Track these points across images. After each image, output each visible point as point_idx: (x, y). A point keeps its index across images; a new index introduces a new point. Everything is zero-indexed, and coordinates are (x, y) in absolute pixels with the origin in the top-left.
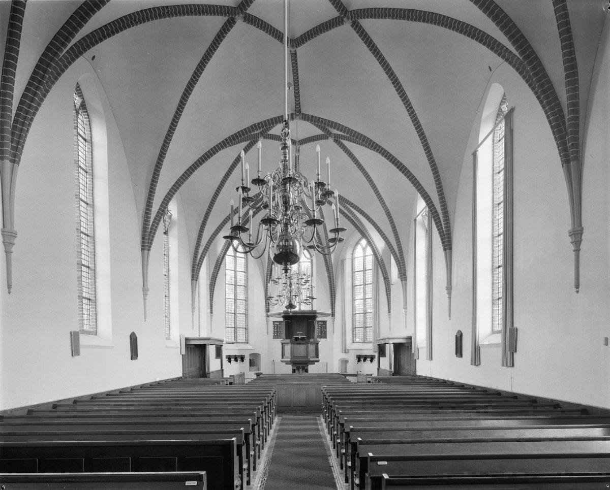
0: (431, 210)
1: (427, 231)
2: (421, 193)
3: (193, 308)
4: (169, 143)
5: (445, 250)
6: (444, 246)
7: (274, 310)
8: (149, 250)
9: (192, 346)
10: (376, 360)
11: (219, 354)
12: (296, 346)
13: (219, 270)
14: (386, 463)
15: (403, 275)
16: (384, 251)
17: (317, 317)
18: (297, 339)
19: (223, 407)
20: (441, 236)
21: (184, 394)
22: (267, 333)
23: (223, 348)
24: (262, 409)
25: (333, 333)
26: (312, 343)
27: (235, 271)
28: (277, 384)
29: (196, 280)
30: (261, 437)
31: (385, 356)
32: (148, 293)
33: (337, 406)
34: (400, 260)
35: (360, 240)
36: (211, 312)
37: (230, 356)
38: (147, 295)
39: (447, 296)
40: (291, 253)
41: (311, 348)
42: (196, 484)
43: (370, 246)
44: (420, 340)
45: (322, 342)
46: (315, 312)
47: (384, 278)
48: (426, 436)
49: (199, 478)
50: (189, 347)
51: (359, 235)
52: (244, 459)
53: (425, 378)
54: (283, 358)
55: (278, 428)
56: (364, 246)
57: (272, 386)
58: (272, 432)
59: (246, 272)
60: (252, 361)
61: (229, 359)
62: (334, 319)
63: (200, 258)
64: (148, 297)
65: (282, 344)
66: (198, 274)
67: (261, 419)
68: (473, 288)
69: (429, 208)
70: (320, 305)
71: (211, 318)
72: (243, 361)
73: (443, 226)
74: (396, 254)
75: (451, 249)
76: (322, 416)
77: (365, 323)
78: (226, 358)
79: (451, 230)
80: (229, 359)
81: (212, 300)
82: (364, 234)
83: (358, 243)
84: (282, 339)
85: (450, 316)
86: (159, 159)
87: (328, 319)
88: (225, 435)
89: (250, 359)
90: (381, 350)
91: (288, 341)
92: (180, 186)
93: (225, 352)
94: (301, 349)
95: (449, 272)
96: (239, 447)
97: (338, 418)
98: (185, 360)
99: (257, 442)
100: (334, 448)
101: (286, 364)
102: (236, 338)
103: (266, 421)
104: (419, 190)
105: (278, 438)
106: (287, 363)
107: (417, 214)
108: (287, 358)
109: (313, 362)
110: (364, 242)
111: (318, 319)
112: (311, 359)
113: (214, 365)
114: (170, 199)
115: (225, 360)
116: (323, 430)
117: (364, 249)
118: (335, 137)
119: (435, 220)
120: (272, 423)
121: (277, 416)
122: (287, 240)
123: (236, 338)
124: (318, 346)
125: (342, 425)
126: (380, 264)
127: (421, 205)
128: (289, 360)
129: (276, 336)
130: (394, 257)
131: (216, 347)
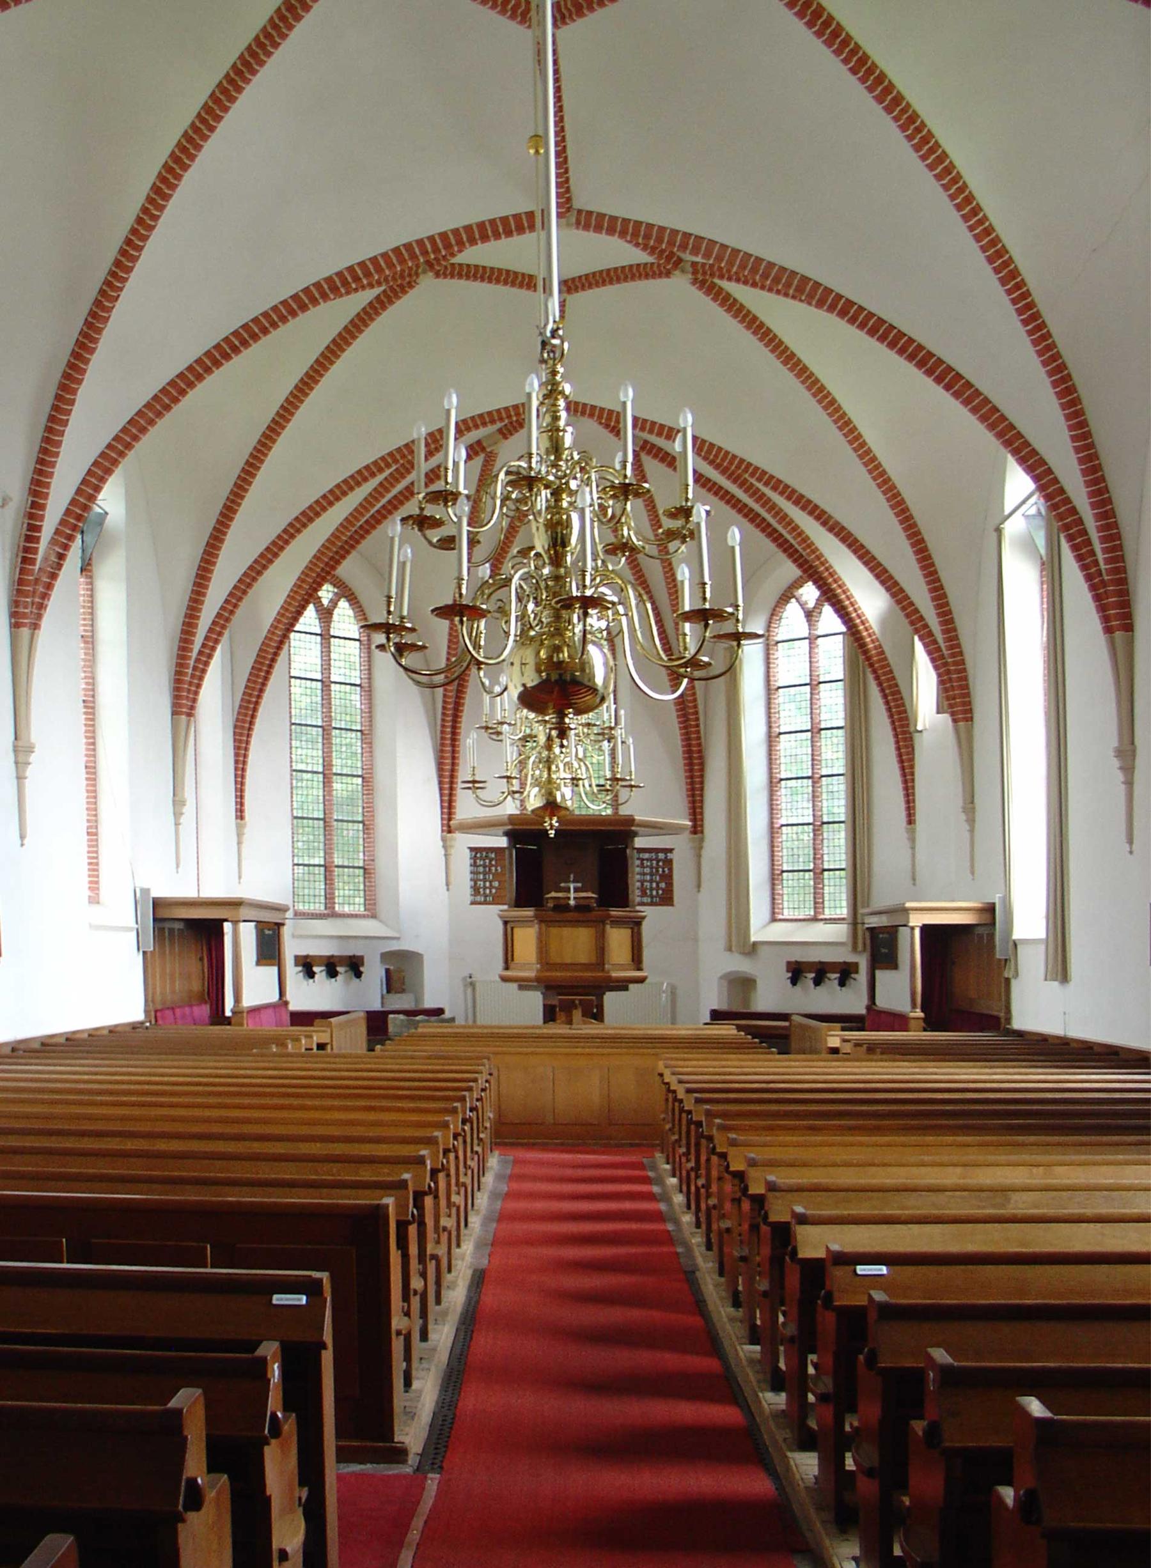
0: (1053, 507)
1: (1043, 564)
2: (1015, 452)
3: (178, 803)
4: (109, 310)
5: (1108, 630)
6: (1106, 619)
7: (467, 808)
8: (35, 626)
9: (180, 926)
10: (862, 977)
11: (269, 949)
12: (554, 931)
13: (266, 679)
14: (884, 1270)
15: (957, 697)
16: (884, 622)
17: (635, 834)
18: (561, 907)
19: (317, 1115)
20: (1093, 588)
21: (172, 1075)
22: (447, 884)
23: (286, 932)
24: (456, 1127)
25: (699, 886)
26: (618, 922)
27: (326, 684)
28: (496, 1054)
29: (190, 715)
30: (415, 1302)
31: (895, 966)
32: (33, 758)
33: (718, 1121)
34: (946, 652)
35: (798, 584)
36: (240, 814)
37: (307, 957)
38: (182, 814)
39: (1120, 777)
40: (575, 682)
41: (618, 939)
42: (304, 1302)
43: (833, 605)
44: (1028, 921)
45: (653, 917)
46: (630, 821)
47: (889, 709)
48: (1020, 1204)
49: (312, 1289)
50: (167, 925)
51: (791, 571)
52: (414, 1264)
53: (1043, 1039)
54: (507, 968)
55: (504, 1188)
56: (811, 605)
57: (478, 1058)
58: (482, 1200)
59: (367, 689)
60: (395, 977)
61: (307, 965)
62: (702, 840)
63: (204, 645)
64: (30, 772)
65: (506, 923)
66: (196, 693)
67: (452, 1156)
68: (1061, 836)
69: (1048, 498)
70: (653, 803)
71: (240, 835)
72: (358, 975)
73: (1100, 557)
74: (930, 634)
75: (1129, 628)
76: (659, 1156)
77: (817, 856)
78: (296, 965)
79: (1131, 580)
80: (307, 965)
81: (242, 784)
82: (813, 569)
83: (786, 596)
84: (505, 907)
85: (1130, 841)
86: (75, 355)
87: (680, 845)
88: (353, 1192)
89: (387, 971)
90: (881, 946)
91: (529, 912)
92: (143, 430)
93: (292, 948)
94: (575, 944)
95: (1125, 705)
96: (402, 1226)
97: (723, 1156)
98: (154, 976)
99: (444, 1222)
100: (709, 1247)
101: (521, 988)
102: (329, 898)
103: (465, 1163)
104: (1007, 444)
105: (503, 1217)
106: (524, 984)
107: (1007, 512)
108: (523, 967)
109: (622, 985)
110: (810, 593)
111: (639, 842)
112: (614, 974)
113: (253, 986)
114: (109, 472)
115: (293, 972)
116: (666, 1198)
117: (811, 615)
118: (695, 273)
119: (1070, 538)
120: (482, 1170)
121: (496, 1153)
122: (558, 649)
123: (329, 898)
124: (639, 934)
125: (740, 1176)
126: (871, 669)
127: (1018, 484)
128: (531, 974)
129: (480, 895)
130: (926, 646)
131: (256, 927)
